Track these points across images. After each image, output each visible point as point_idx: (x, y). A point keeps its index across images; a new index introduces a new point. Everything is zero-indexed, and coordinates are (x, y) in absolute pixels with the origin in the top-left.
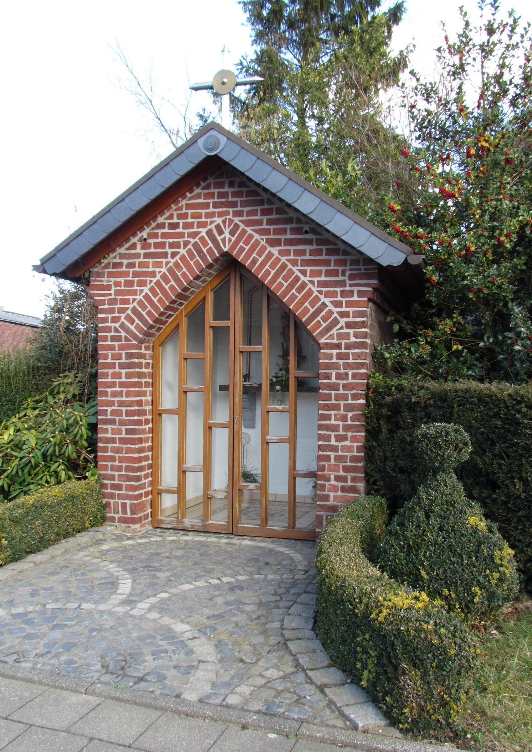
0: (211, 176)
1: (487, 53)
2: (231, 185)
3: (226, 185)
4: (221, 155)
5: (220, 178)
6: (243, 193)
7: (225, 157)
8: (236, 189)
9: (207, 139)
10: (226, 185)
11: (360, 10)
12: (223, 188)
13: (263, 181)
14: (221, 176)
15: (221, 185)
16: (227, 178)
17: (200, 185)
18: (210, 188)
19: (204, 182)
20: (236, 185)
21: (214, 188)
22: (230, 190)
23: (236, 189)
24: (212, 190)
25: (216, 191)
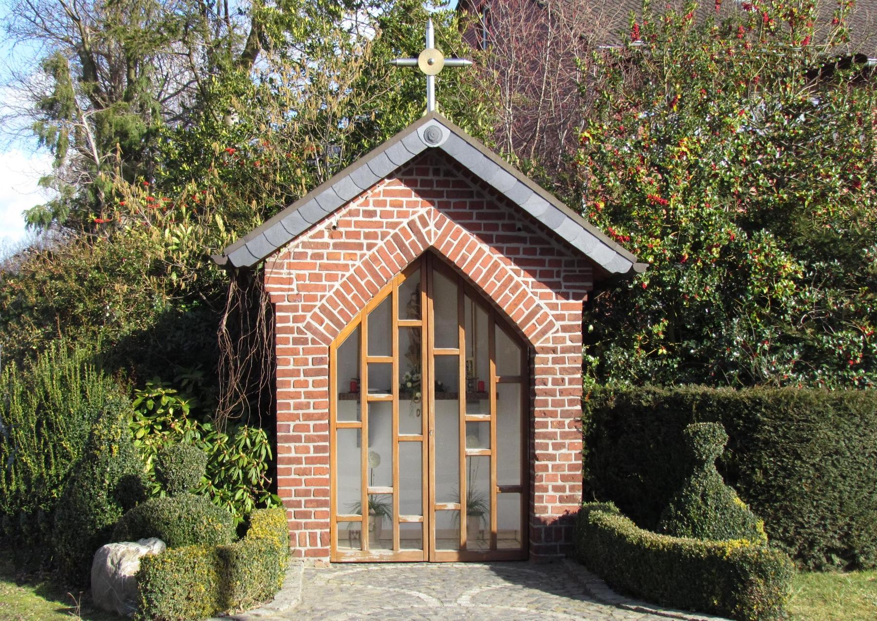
2: (436, 172)
8: (441, 178)
21: (417, 175)
22: (435, 178)
24: (414, 177)
25: (419, 178)
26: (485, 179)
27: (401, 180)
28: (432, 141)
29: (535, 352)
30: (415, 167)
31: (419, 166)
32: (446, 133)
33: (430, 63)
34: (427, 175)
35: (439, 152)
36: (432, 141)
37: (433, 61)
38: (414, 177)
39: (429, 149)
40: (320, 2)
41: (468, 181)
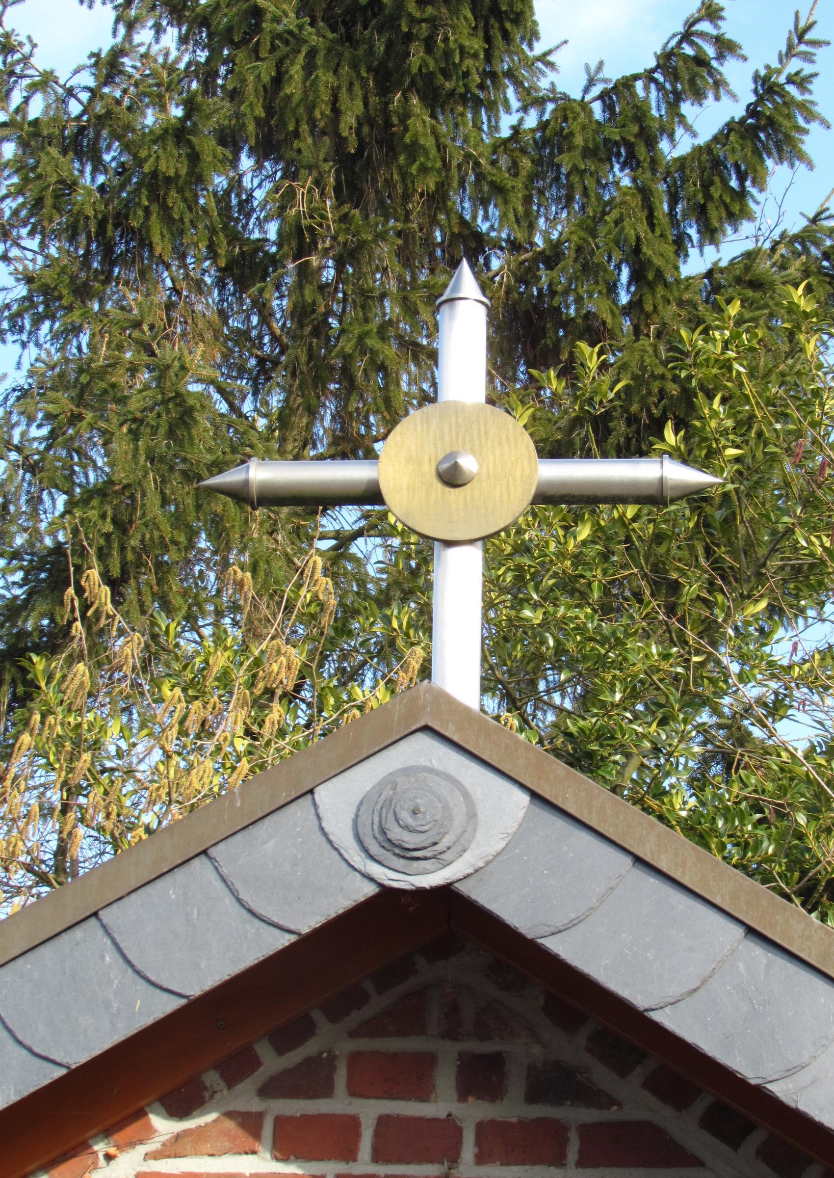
0: (334, 1017)
1: (405, 594)
2: (480, 1077)
3: (445, 1080)
4: (463, 888)
5: (402, 1033)
6: (563, 1143)
7: (511, 904)
8: (511, 1109)
9: (390, 781)
10: (445, 1080)
11: (643, 228)
12: (423, 1094)
13: (790, 1072)
14: (407, 1018)
15: (414, 1078)
16: (451, 1034)
17: (255, 1063)
18: (326, 1090)
19: (281, 1049)
20: (516, 1083)
21: (354, 1091)
22: (472, 1113)
23: (511, 1109)
24: (339, 1104)
25: (369, 1111)
26: (751, 1073)
27: (250, 1124)
28: (407, 854)
29: (48, 659)
30: (345, 1047)
31: (366, 1044)
32: (501, 809)
33: (452, 478)
34: (422, 1091)
35: (448, 917)
36: (407, 854)
37: (468, 463)
38: (339, 1104)
39: (387, 896)
40: (796, 732)
41: (685, 1128)
